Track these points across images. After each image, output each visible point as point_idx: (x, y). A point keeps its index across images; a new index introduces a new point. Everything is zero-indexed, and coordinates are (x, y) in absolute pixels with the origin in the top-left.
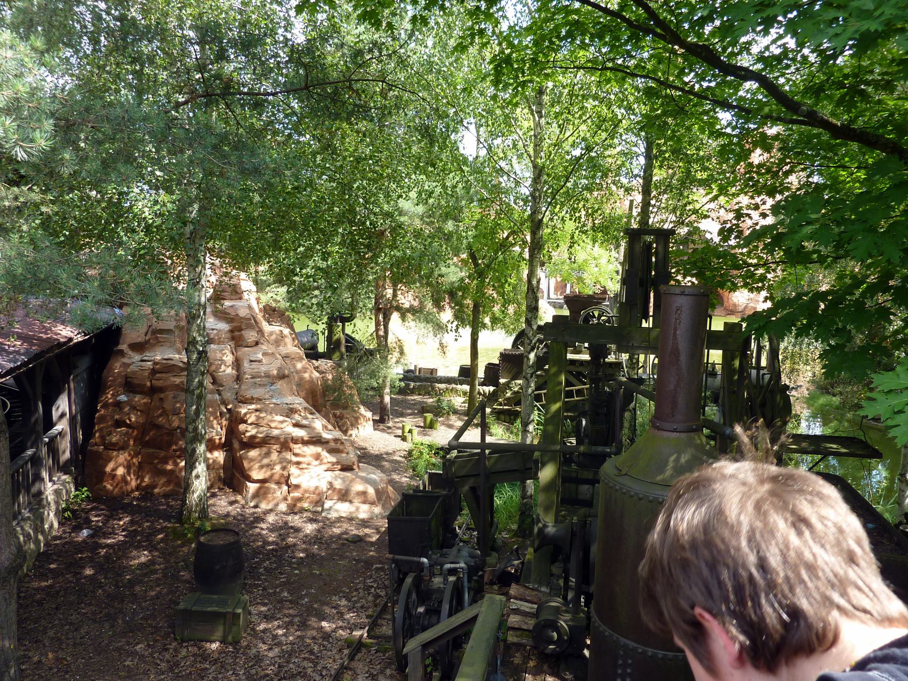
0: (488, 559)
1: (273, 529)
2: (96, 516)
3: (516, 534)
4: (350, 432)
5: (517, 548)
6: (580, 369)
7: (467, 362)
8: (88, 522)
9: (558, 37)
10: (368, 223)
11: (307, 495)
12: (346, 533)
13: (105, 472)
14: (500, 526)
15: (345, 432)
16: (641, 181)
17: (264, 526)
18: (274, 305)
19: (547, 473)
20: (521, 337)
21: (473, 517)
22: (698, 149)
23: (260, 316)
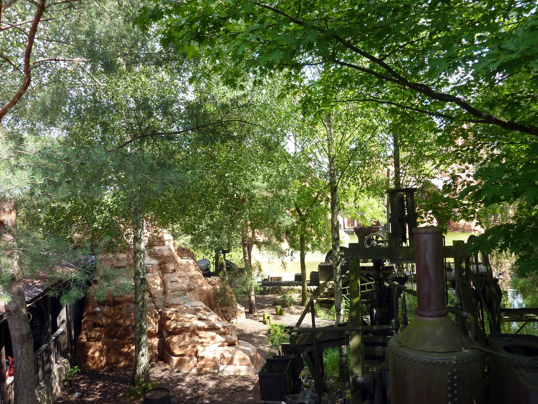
0: (322, 397)
1: (189, 385)
2: (83, 384)
3: (338, 380)
4: (232, 321)
5: (340, 391)
6: (368, 272)
7: (299, 272)
8: (78, 387)
9: (337, 85)
10: (235, 195)
11: (209, 362)
12: (233, 386)
13: (88, 356)
14: (328, 375)
15: (229, 321)
16: (392, 159)
17: (183, 384)
18: (184, 247)
19: (355, 341)
20: (330, 255)
21: (310, 371)
22: (425, 139)
23: (175, 254)
